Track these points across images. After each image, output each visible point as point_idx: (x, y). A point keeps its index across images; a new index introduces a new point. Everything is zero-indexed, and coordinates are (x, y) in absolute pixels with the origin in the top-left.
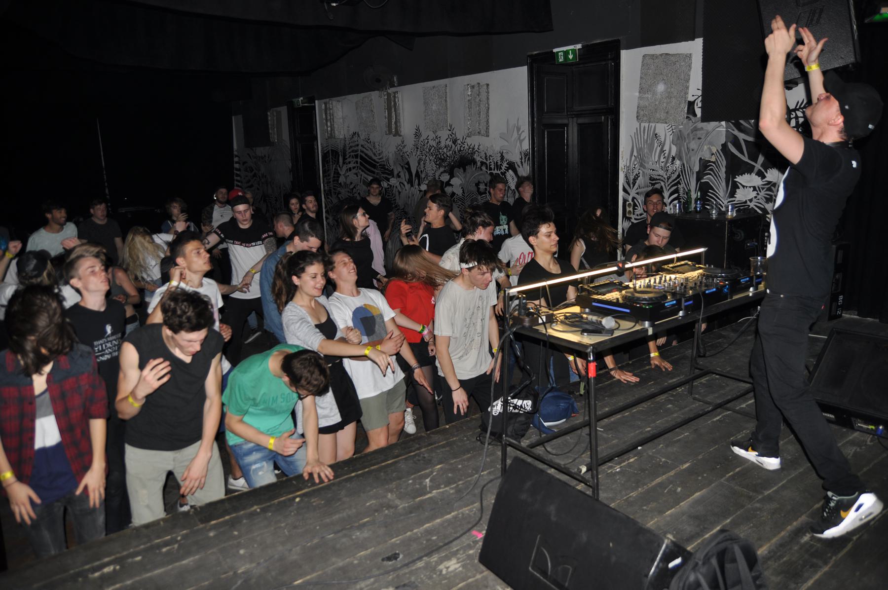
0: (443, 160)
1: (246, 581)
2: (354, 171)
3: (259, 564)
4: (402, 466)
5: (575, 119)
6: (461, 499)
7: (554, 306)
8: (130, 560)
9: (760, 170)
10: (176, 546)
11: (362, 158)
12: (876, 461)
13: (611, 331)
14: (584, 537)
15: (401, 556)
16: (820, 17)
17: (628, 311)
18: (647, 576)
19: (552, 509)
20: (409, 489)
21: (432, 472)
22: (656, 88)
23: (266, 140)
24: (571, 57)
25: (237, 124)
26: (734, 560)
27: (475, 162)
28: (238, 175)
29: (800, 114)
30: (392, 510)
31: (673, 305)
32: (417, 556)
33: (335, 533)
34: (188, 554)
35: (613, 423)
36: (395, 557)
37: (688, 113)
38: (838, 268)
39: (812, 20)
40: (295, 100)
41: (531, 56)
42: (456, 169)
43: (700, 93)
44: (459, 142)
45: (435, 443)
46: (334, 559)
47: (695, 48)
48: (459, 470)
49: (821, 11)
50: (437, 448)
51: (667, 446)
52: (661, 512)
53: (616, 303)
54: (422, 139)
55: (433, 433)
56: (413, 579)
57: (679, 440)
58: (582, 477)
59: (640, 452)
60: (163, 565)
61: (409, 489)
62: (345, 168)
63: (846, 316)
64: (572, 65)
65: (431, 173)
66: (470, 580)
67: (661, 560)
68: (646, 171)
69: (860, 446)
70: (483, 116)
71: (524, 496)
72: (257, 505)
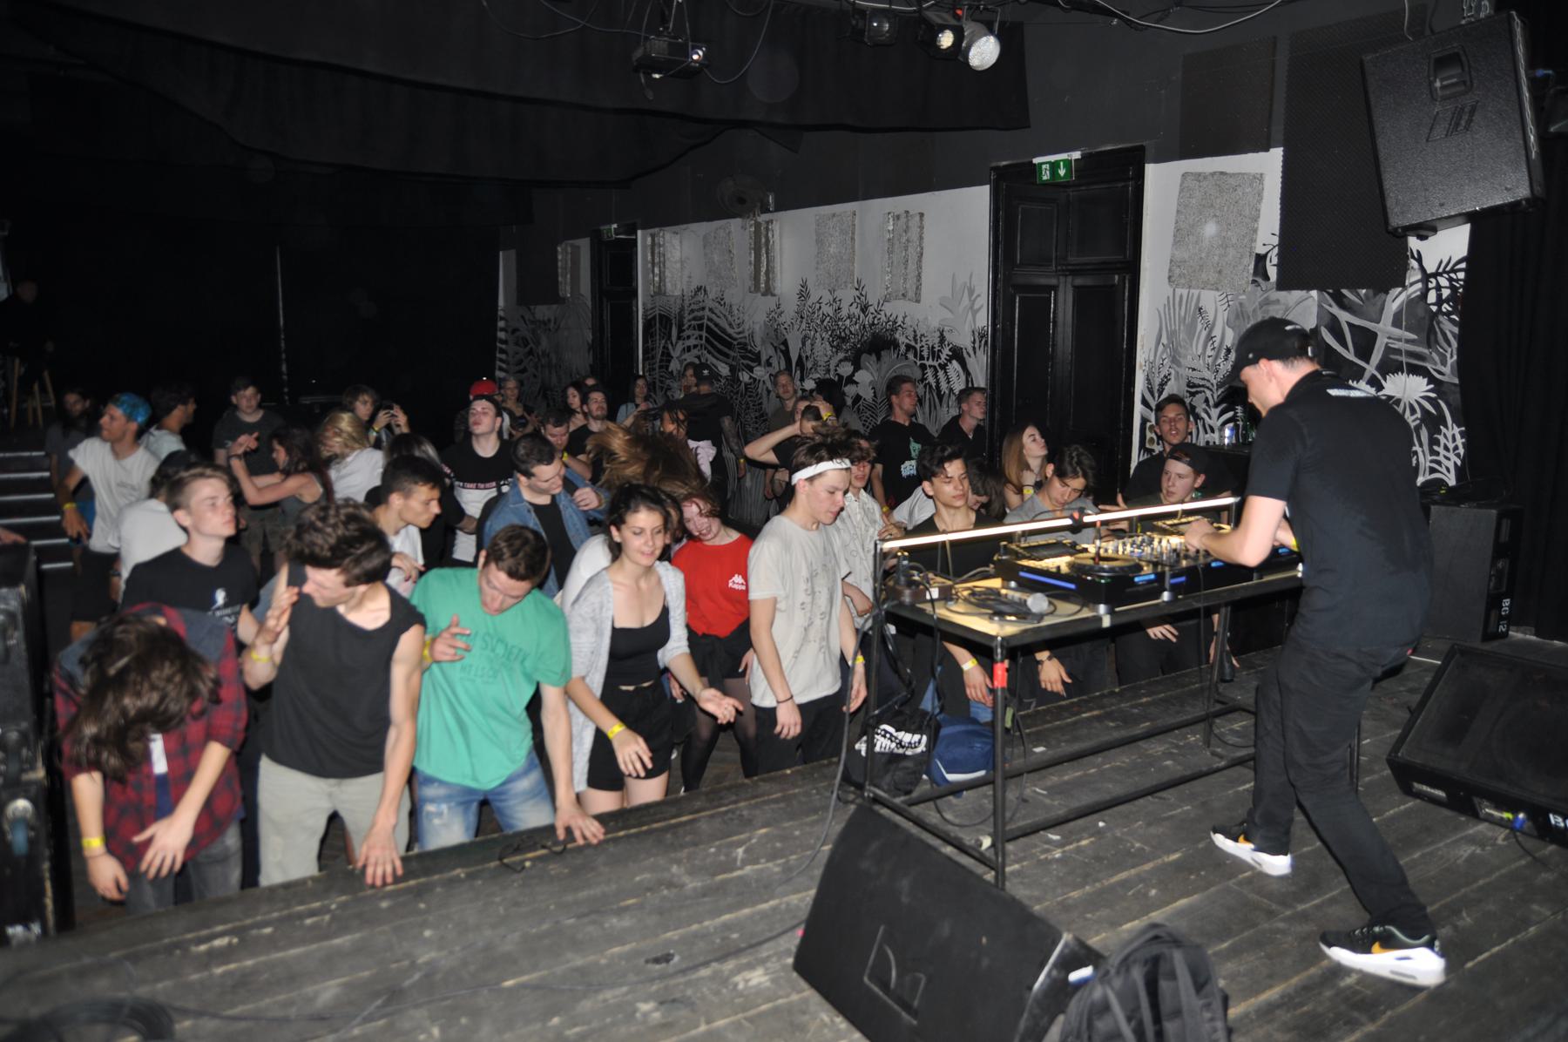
0: (844, 340)
1: (427, 976)
2: (695, 352)
3: (451, 953)
4: (704, 826)
5: (1070, 279)
6: (788, 881)
7: (959, 575)
8: (254, 932)
9: (1373, 376)
10: (327, 917)
11: (709, 330)
12: (1503, 871)
13: (1041, 617)
14: (945, 929)
15: (676, 959)
16: (1470, 121)
17: (1072, 586)
18: (1030, 988)
19: (905, 884)
20: (708, 861)
21: (750, 839)
22: (1207, 233)
23: (553, 297)
24: (1062, 172)
25: (506, 264)
26: (1172, 976)
27: (896, 345)
28: (502, 351)
29: (1443, 282)
30: (674, 891)
31: (1150, 582)
32: (702, 959)
33: (579, 917)
34: (344, 929)
35: (1067, 783)
36: (667, 958)
37: (1256, 273)
38: (1499, 551)
39: (1457, 124)
40: (604, 228)
41: (996, 169)
42: (864, 356)
43: (1276, 240)
44: (871, 309)
45: (762, 795)
46: (569, 955)
47: (1269, 165)
48: (796, 838)
49: (1473, 111)
50: (765, 803)
51: (1149, 824)
52: (1114, 924)
53: (1057, 574)
54: (810, 302)
55: (764, 780)
56: (689, 992)
57: (1172, 817)
58: (981, 854)
59: (1099, 832)
60: (303, 942)
61: (708, 861)
62: (680, 346)
63: (1516, 635)
64: (1064, 186)
65: (822, 361)
66: (780, 1001)
67: (1055, 965)
68: (1181, 371)
69: (1483, 846)
70: (912, 266)
71: (865, 865)
72: (462, 866)
